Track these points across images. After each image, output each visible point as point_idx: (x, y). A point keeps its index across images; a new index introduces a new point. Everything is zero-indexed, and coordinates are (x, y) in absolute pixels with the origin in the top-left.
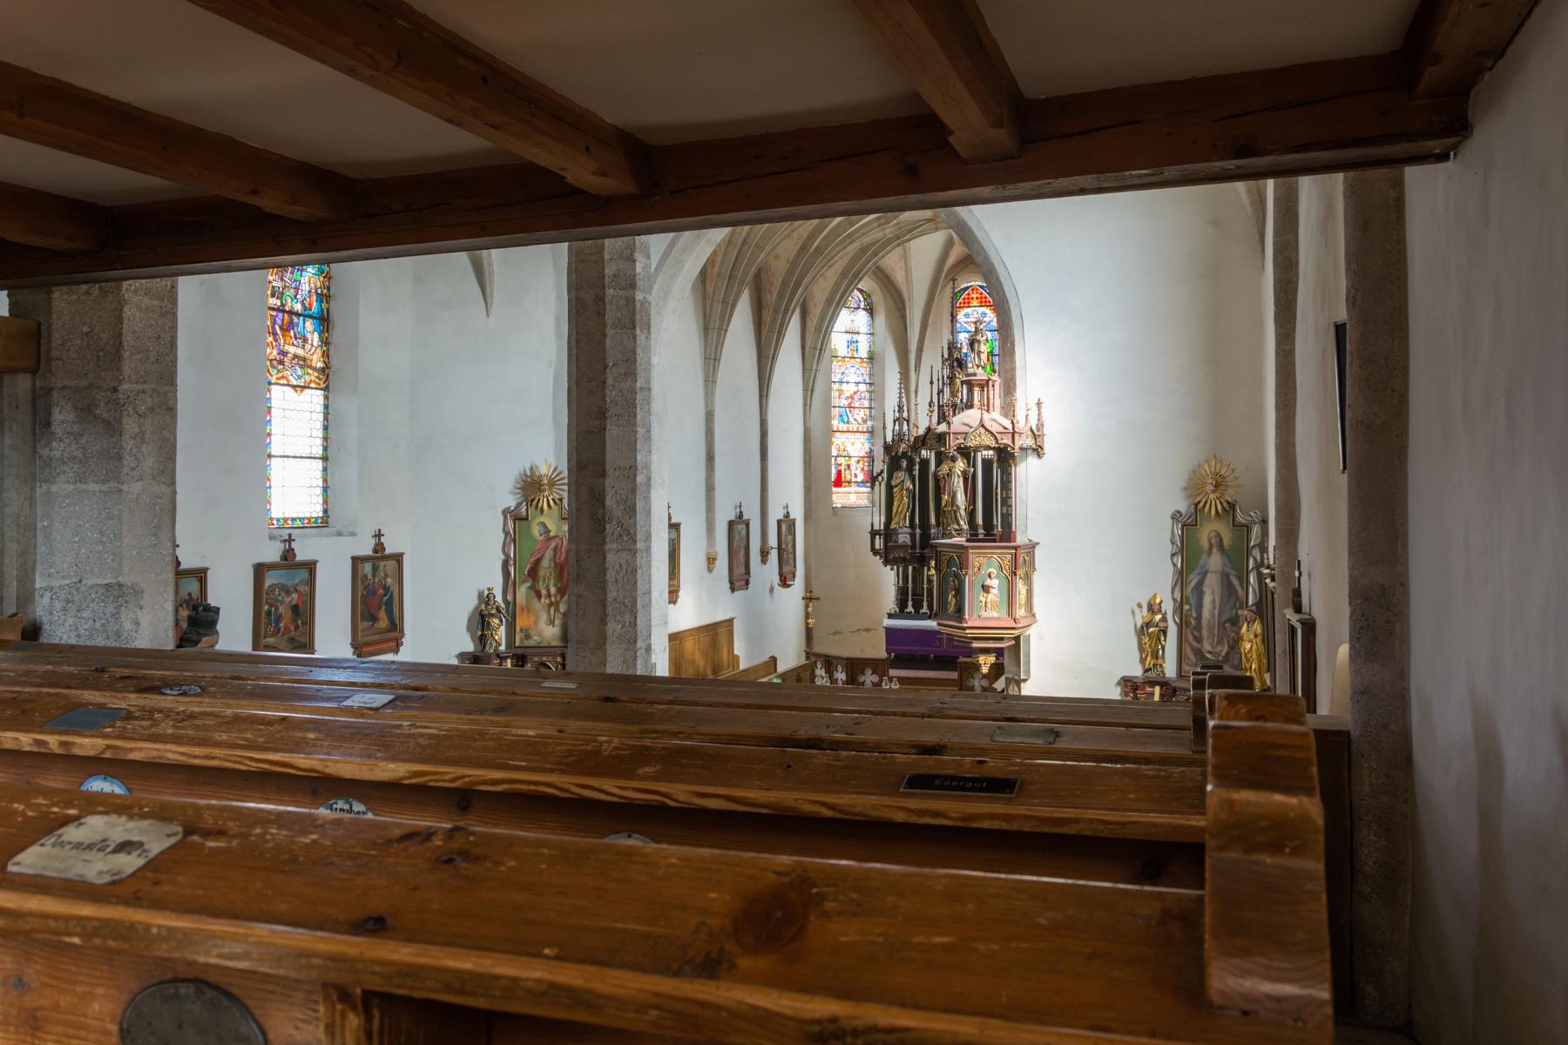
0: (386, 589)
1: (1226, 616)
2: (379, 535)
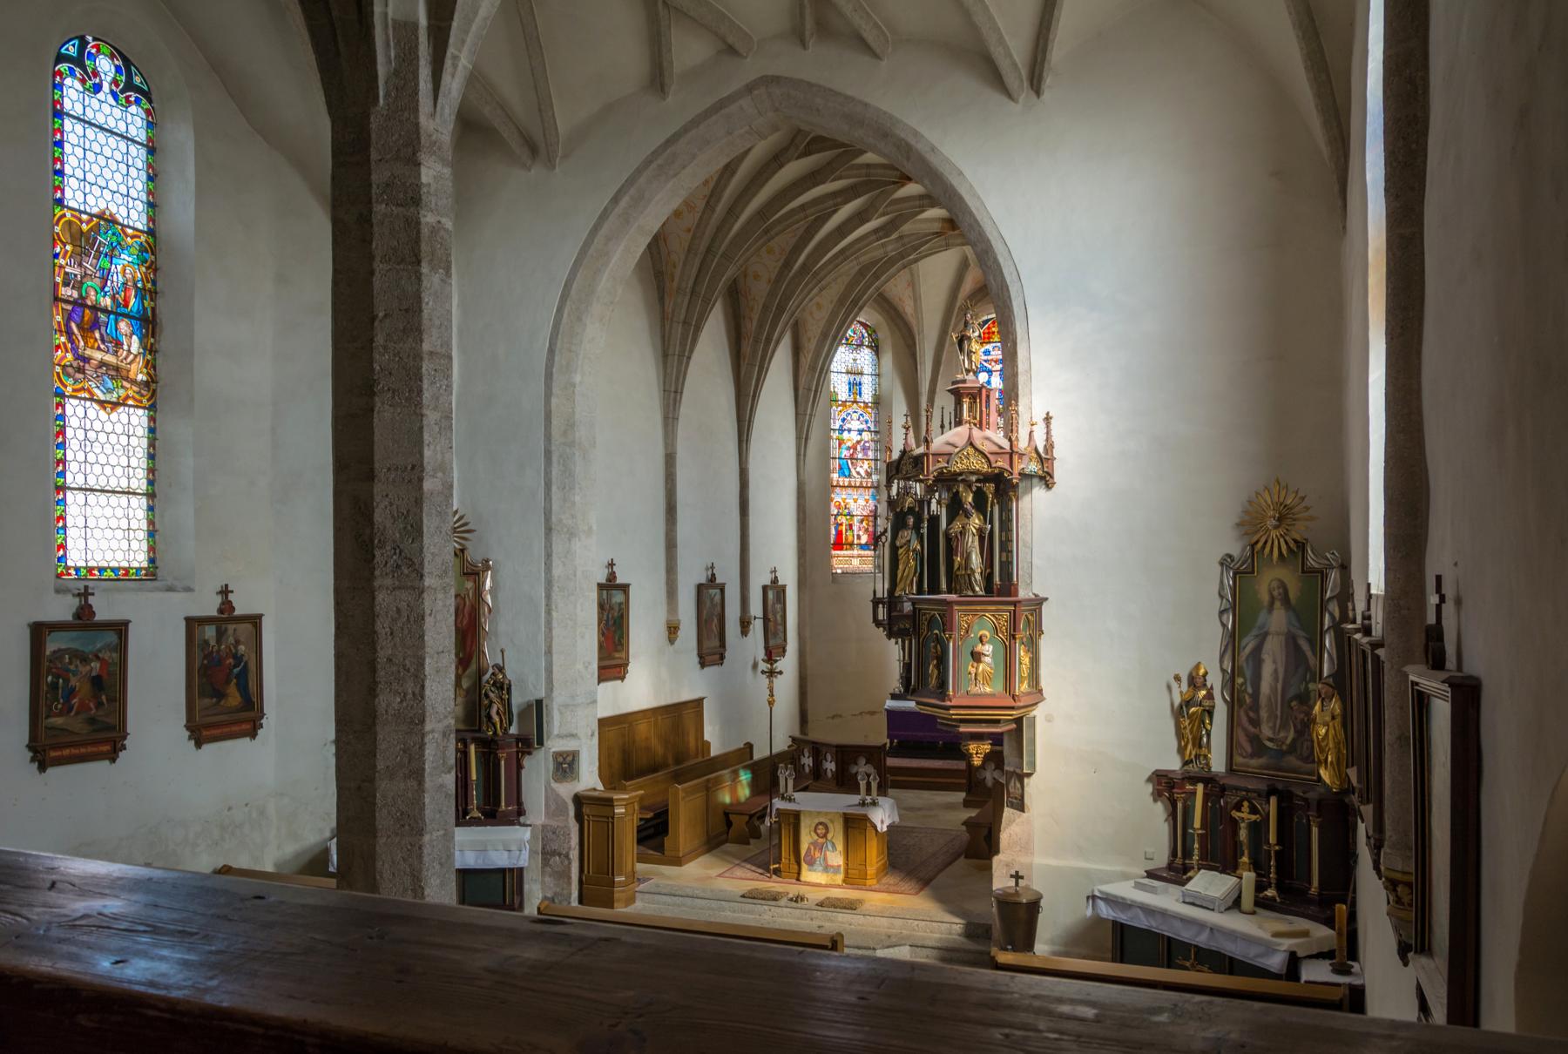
0: (238, 659)
1: (1292, 692)
2: (225, 591)
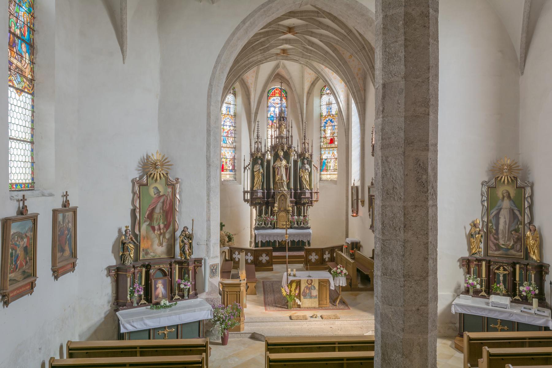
1: (512, 229)
2: (66, 195)
